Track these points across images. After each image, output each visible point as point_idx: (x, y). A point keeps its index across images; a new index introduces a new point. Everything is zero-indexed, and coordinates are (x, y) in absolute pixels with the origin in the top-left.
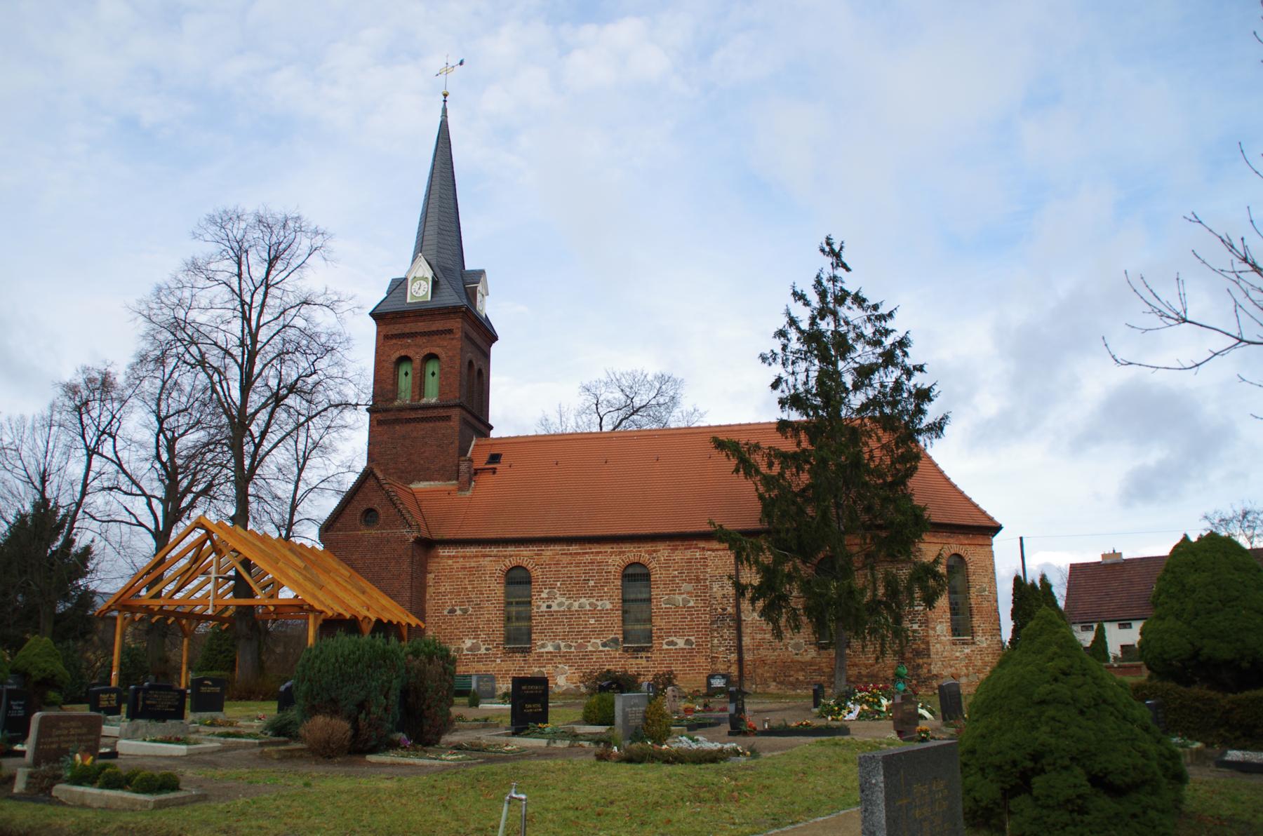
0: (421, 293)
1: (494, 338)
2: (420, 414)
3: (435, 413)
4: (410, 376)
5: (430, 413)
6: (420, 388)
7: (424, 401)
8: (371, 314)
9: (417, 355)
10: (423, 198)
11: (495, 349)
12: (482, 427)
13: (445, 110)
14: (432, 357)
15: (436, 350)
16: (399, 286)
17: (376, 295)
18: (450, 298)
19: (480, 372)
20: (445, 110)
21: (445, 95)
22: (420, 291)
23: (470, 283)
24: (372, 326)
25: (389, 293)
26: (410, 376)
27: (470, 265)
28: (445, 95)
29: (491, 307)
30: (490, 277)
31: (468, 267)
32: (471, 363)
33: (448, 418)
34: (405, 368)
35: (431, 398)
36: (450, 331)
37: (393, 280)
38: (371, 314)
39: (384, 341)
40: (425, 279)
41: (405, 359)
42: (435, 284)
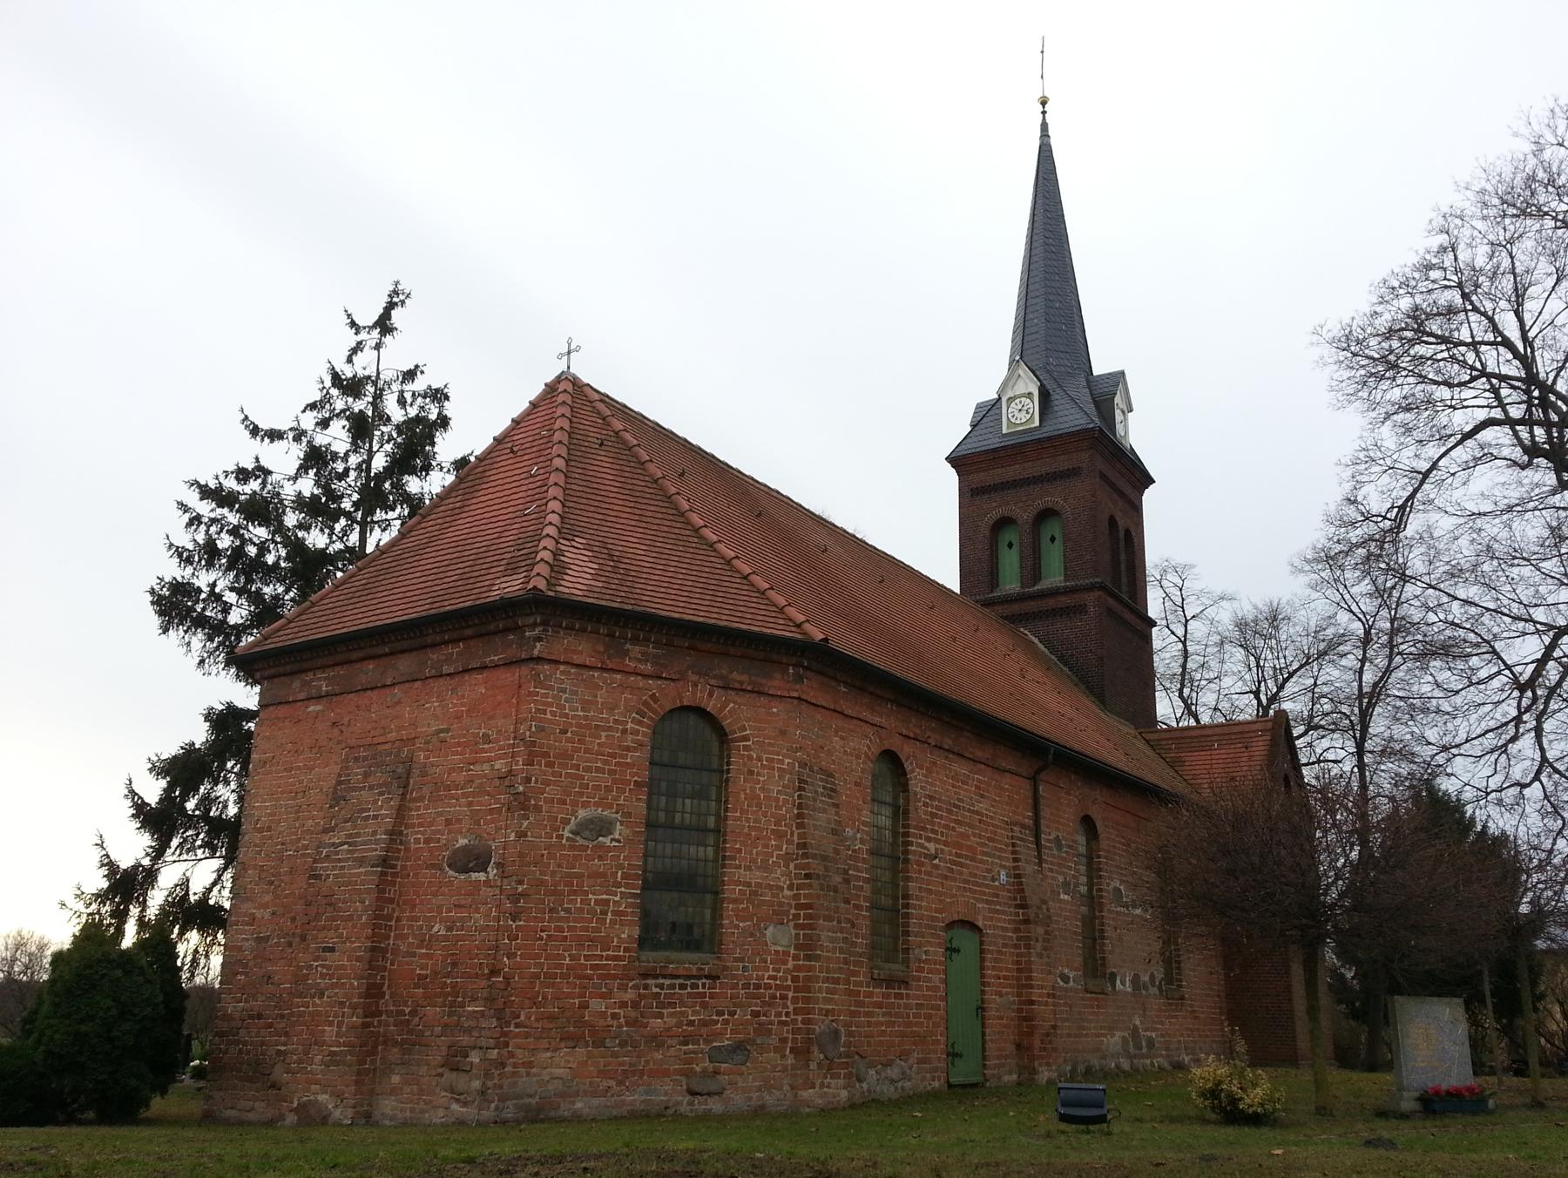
0: (1023, 417)
1: (1148, 480)
2: (1032, 606)
3: (1064, 601)
4: (1015, 548)
5: (1051, 603)
6: (1033, 570)
7: (1045, 584)
8: (1122, 373)
9: (1025, 516)
10: (1024, 240)
11: (1149, 497)
12: (1140, 626)
13: (1044, 127)
14: (1046, 514)
15: (1047, 501)
16: (987, 414)
17: (957, 429)
18: (1071, 418)
19: (1128, 532)
20: (1044, 127)
21: (1044, 103)
22: (1022, 415)
23: (1107, 395)
24: (951, 478)
25: (974, 426)
26: (1015, 548)
27: (1101, 365)
28: (1044, 103)
29: (1142, 433)
30: (1136, 387)
31: (1098, 369)
32: (1112, 521)
33: (1080, 609)
34: (1009, 535)
35: (1054, 577)
36: (1073, 473)
37: (979, 406)
38: (1122, 373)
39: (970, 496)
40: (1029, 395)
41: (1004, 522)
42: (1045, 396)
